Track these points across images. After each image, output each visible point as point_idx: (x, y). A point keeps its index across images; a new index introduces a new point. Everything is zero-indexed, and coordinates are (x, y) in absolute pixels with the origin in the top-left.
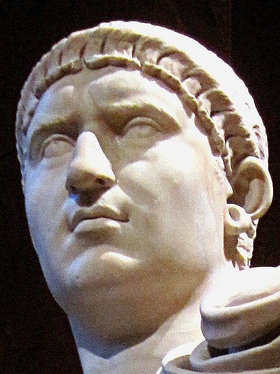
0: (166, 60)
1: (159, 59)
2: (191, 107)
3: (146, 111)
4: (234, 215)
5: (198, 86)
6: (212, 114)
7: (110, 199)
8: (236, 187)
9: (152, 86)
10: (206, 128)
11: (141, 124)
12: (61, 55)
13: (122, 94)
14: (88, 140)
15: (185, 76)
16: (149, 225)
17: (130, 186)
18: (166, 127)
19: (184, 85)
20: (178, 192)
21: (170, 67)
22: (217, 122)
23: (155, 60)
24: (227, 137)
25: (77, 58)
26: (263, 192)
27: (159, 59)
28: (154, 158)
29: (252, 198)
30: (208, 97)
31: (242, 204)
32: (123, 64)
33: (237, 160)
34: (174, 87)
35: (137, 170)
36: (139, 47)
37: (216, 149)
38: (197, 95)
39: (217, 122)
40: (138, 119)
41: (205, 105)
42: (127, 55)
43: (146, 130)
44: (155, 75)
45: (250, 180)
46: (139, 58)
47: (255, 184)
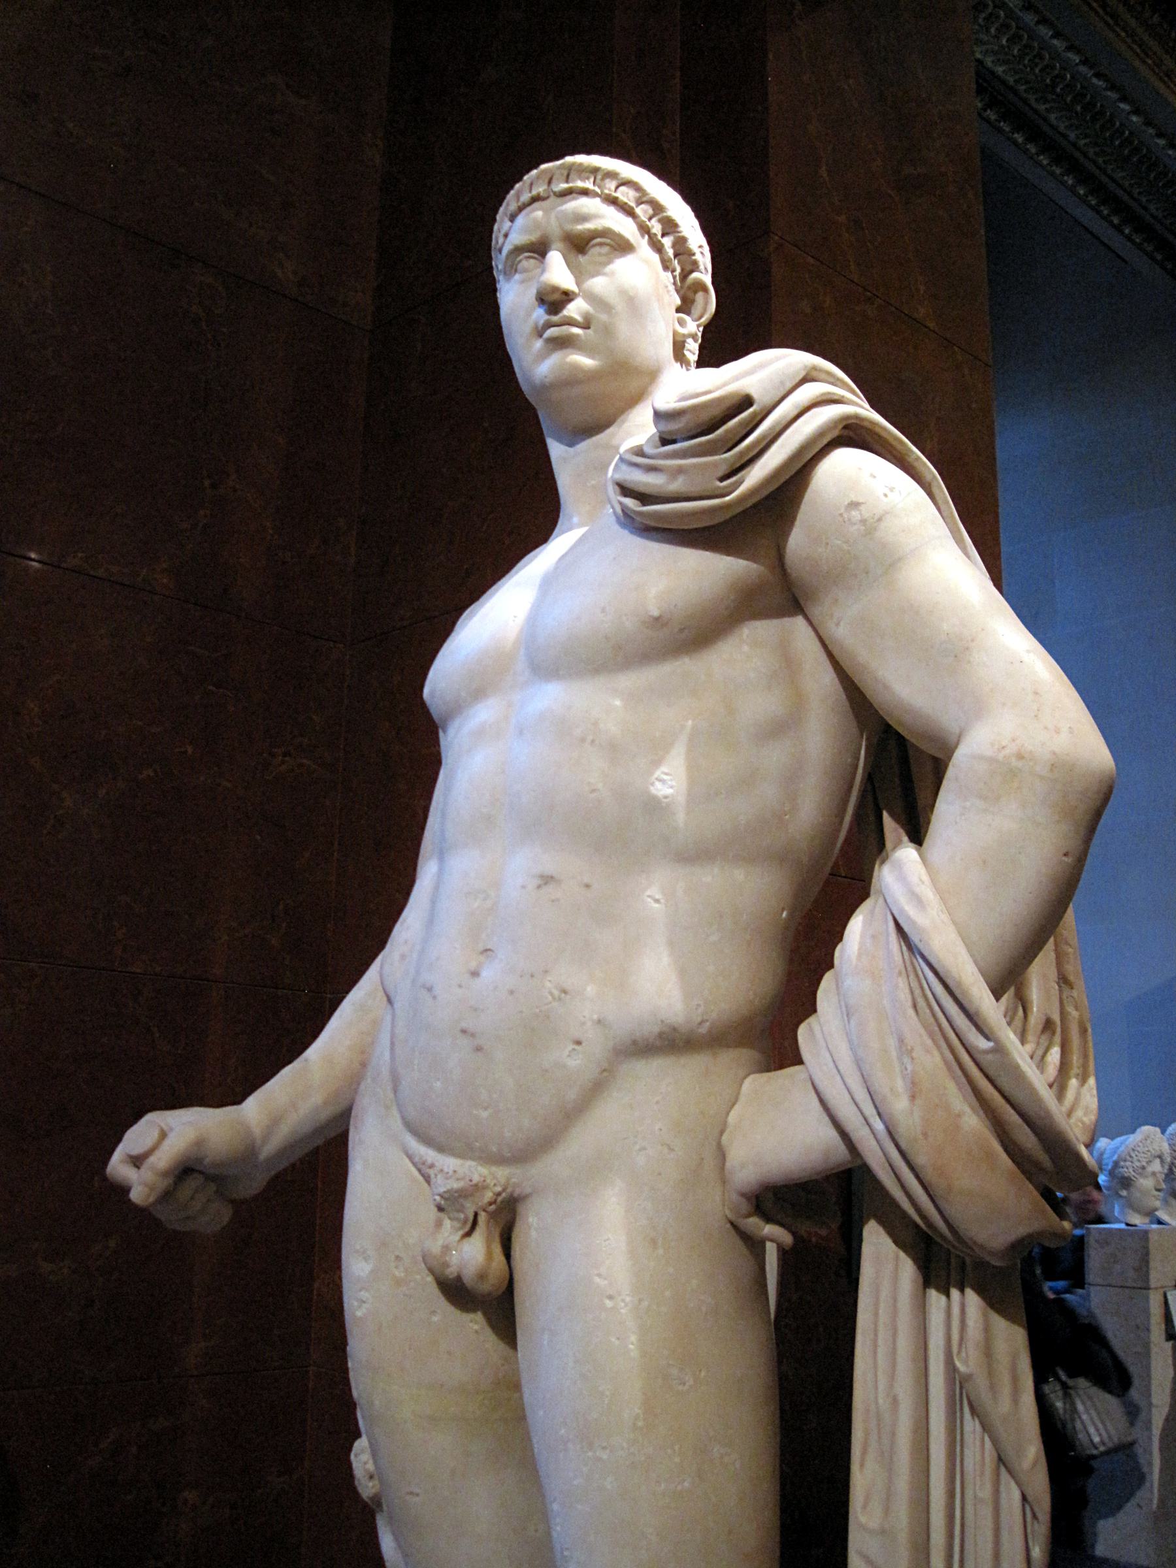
0: (622, 188)
1: (617, 188)
2: (644, 230)
3: (605, 233)
4: (681, 323)
5: (651, 212)
6: (663, 235)
7: (574, 309)
8: (684, 299)
9: (611, 211)
10: (658, 248)
11: (601, 244)
12: (531, 184)
13: (584, 218)
14: (555, 258)
15: (639, 202)
16: (608, 331)
17: (591, 298)
18: (623, 247)
19: (639, 211)
20: (633, 303)
21: (626, 195)
22: (667, 242)
23: (613, 188)
24: (676, 256)
25: (545, 187)
26: (706, 303)
27: (617, 188)
28: (613, 274)
29: (697, 308)
30: (659, 221)
31: (688, 314)
32: (585, 192)
33: (685, 275)
34: (629, 212)
35: (598, 284)
36: (599, 177)
37: (666, 266)
38: (650, 219)
39: (667, 242)
40: (598, 240)
41: (656, 228)
42: (588, 185)
43: (605, 249)
44: (613, 201)
45: (695, 292)
46: (599, 187)
47: (700, 296)
